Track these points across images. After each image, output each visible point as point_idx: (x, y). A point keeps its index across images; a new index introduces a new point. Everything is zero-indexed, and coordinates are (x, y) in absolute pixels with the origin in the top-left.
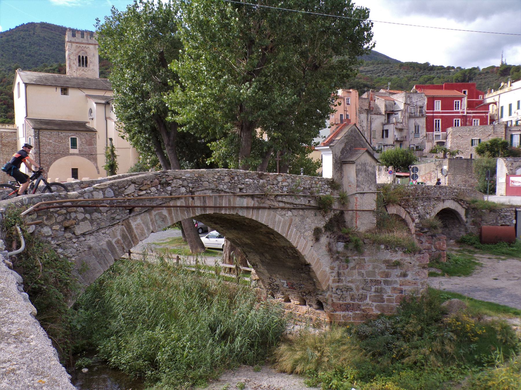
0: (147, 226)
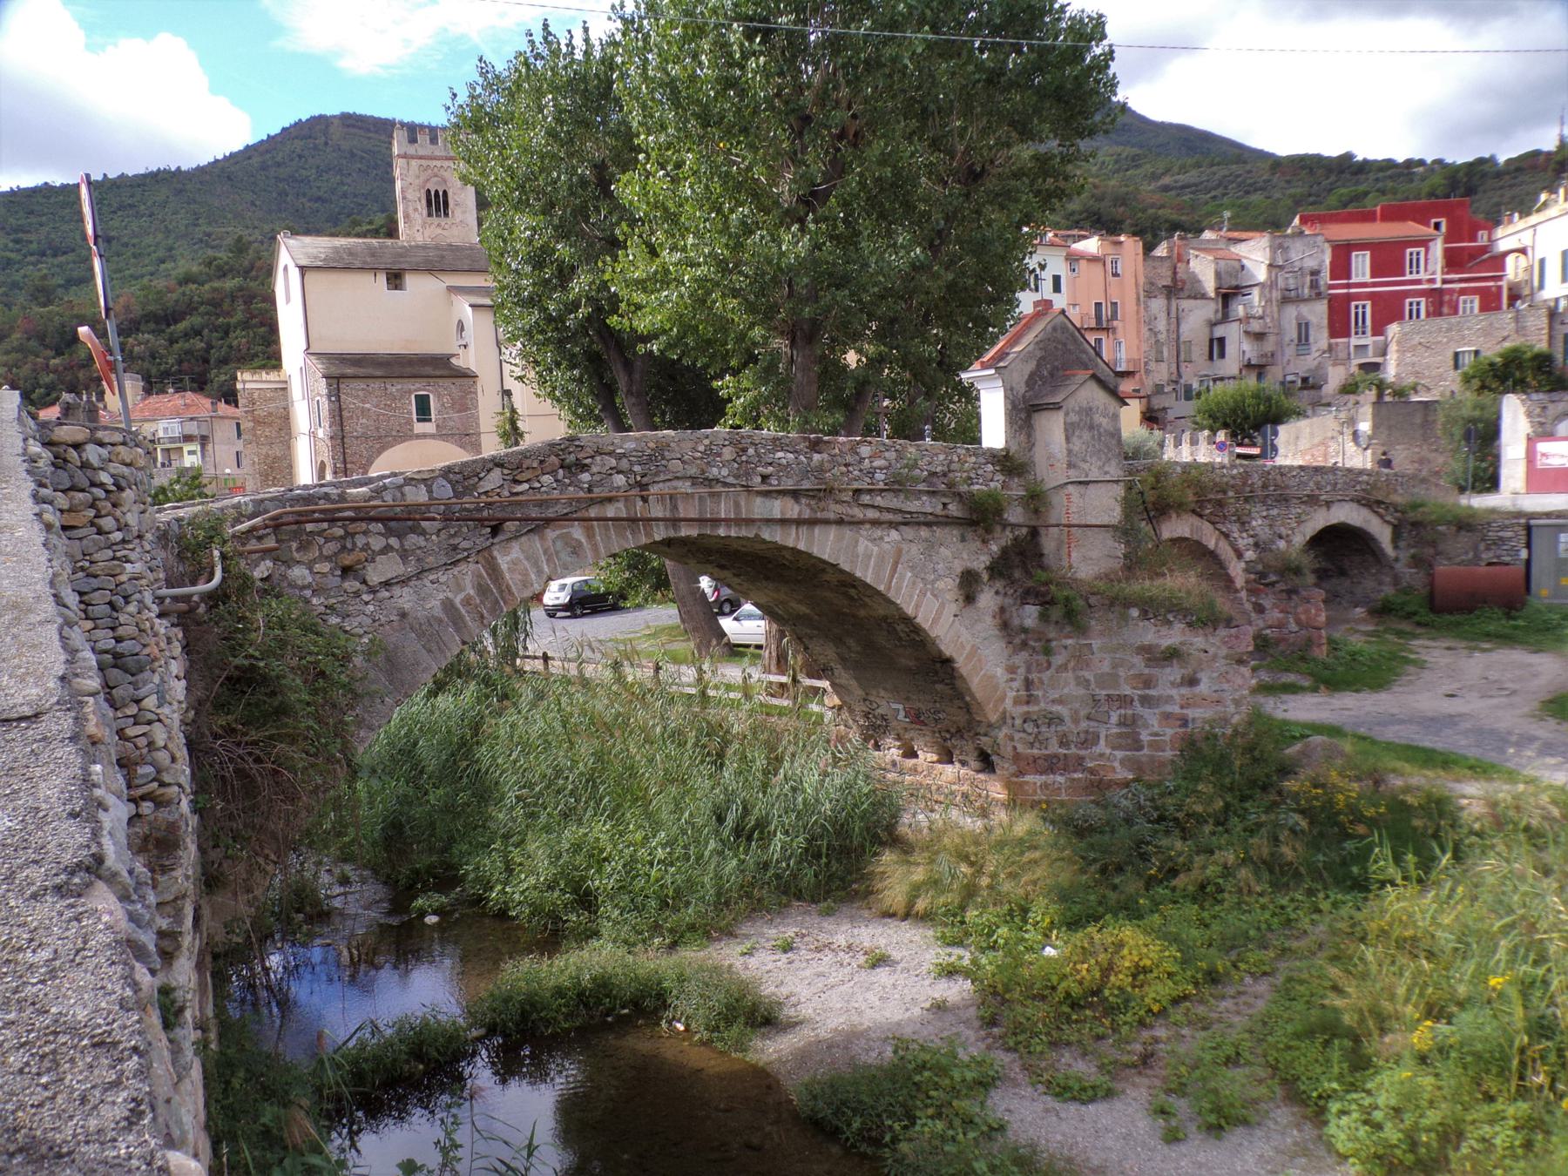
0: (536, 564)
